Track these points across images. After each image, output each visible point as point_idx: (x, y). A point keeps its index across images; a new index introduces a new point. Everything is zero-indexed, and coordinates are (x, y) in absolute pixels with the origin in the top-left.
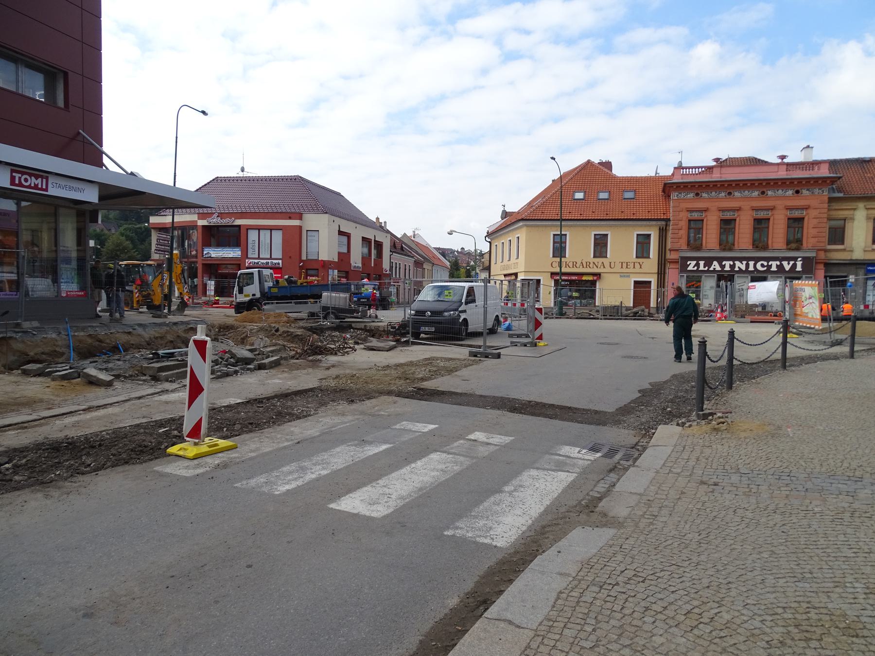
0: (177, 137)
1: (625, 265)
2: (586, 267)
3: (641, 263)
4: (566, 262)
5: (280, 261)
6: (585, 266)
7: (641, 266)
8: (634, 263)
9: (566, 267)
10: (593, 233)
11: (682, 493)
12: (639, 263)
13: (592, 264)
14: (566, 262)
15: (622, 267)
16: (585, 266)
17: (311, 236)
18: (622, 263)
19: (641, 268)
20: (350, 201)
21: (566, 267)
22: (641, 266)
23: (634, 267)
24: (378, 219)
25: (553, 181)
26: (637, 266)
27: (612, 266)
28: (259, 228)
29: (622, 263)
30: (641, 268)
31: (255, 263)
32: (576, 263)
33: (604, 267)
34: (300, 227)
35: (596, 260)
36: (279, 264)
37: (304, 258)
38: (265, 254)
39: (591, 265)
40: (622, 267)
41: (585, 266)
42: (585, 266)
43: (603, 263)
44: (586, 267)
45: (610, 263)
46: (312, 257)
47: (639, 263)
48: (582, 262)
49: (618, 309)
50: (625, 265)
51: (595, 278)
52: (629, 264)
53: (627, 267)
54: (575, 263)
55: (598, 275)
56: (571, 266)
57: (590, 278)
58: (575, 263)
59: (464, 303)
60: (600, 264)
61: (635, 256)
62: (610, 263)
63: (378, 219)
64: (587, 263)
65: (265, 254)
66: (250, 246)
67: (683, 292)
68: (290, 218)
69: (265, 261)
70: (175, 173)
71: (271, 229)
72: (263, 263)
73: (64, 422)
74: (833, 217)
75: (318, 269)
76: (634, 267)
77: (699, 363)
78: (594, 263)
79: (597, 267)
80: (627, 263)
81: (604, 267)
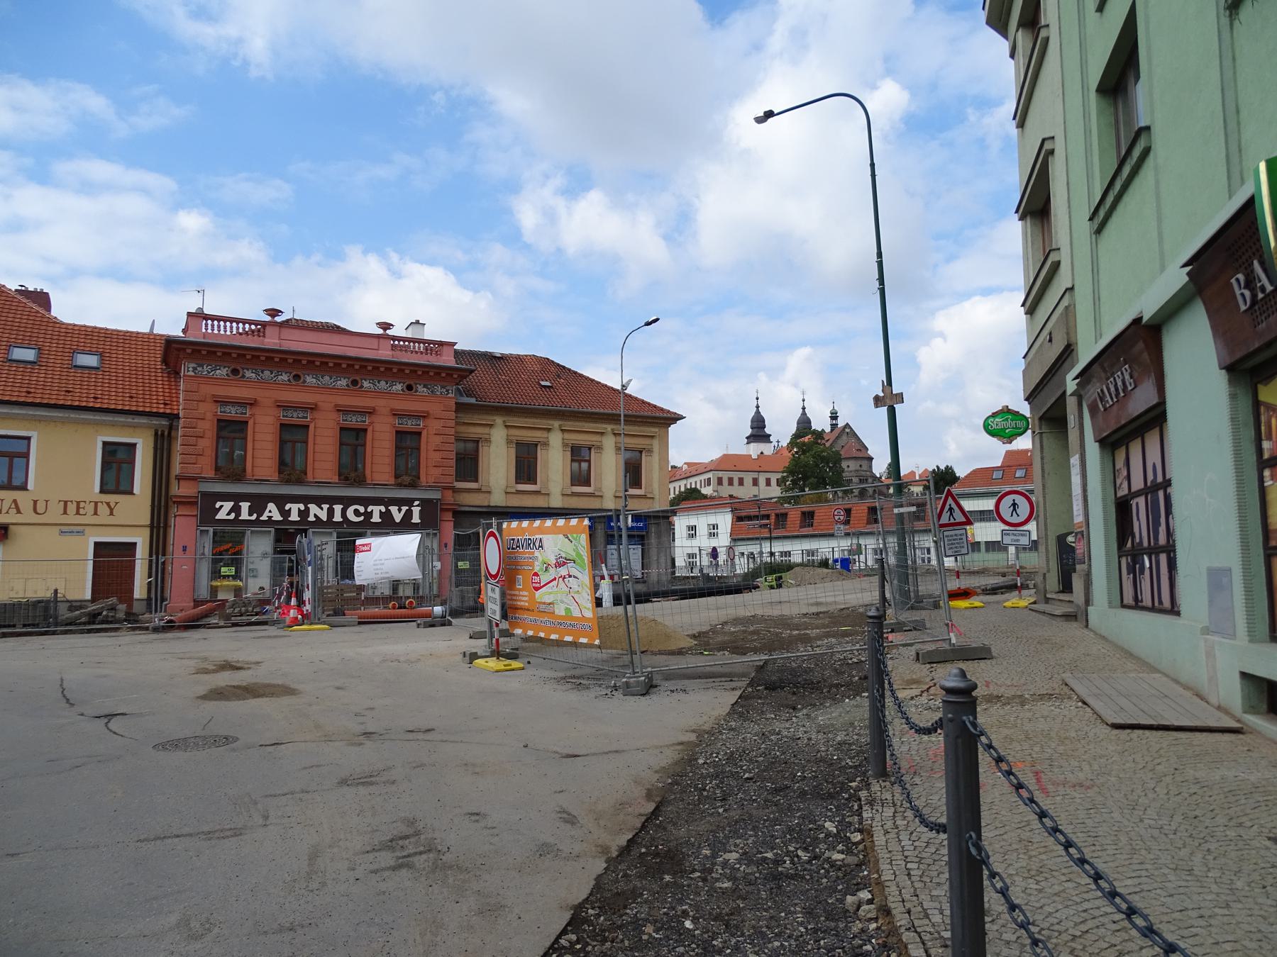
1: (72, 508)
8: (96, 503)
12: (108, 504)
15: (65, 513)
18: (66, 502)
19: (111, 514)
23: (96, 513)
29: (66, 502)
30: (111, 514)
40: (65, 513)
43: (15, 501)
45: (35, 502)
47: (108, 504)
50: (72, 508)
52: (82, 505)
53: (78, 513)
62: (35, 502)
76: (96, 513)
80: (78, 503)
81: (19, 512)
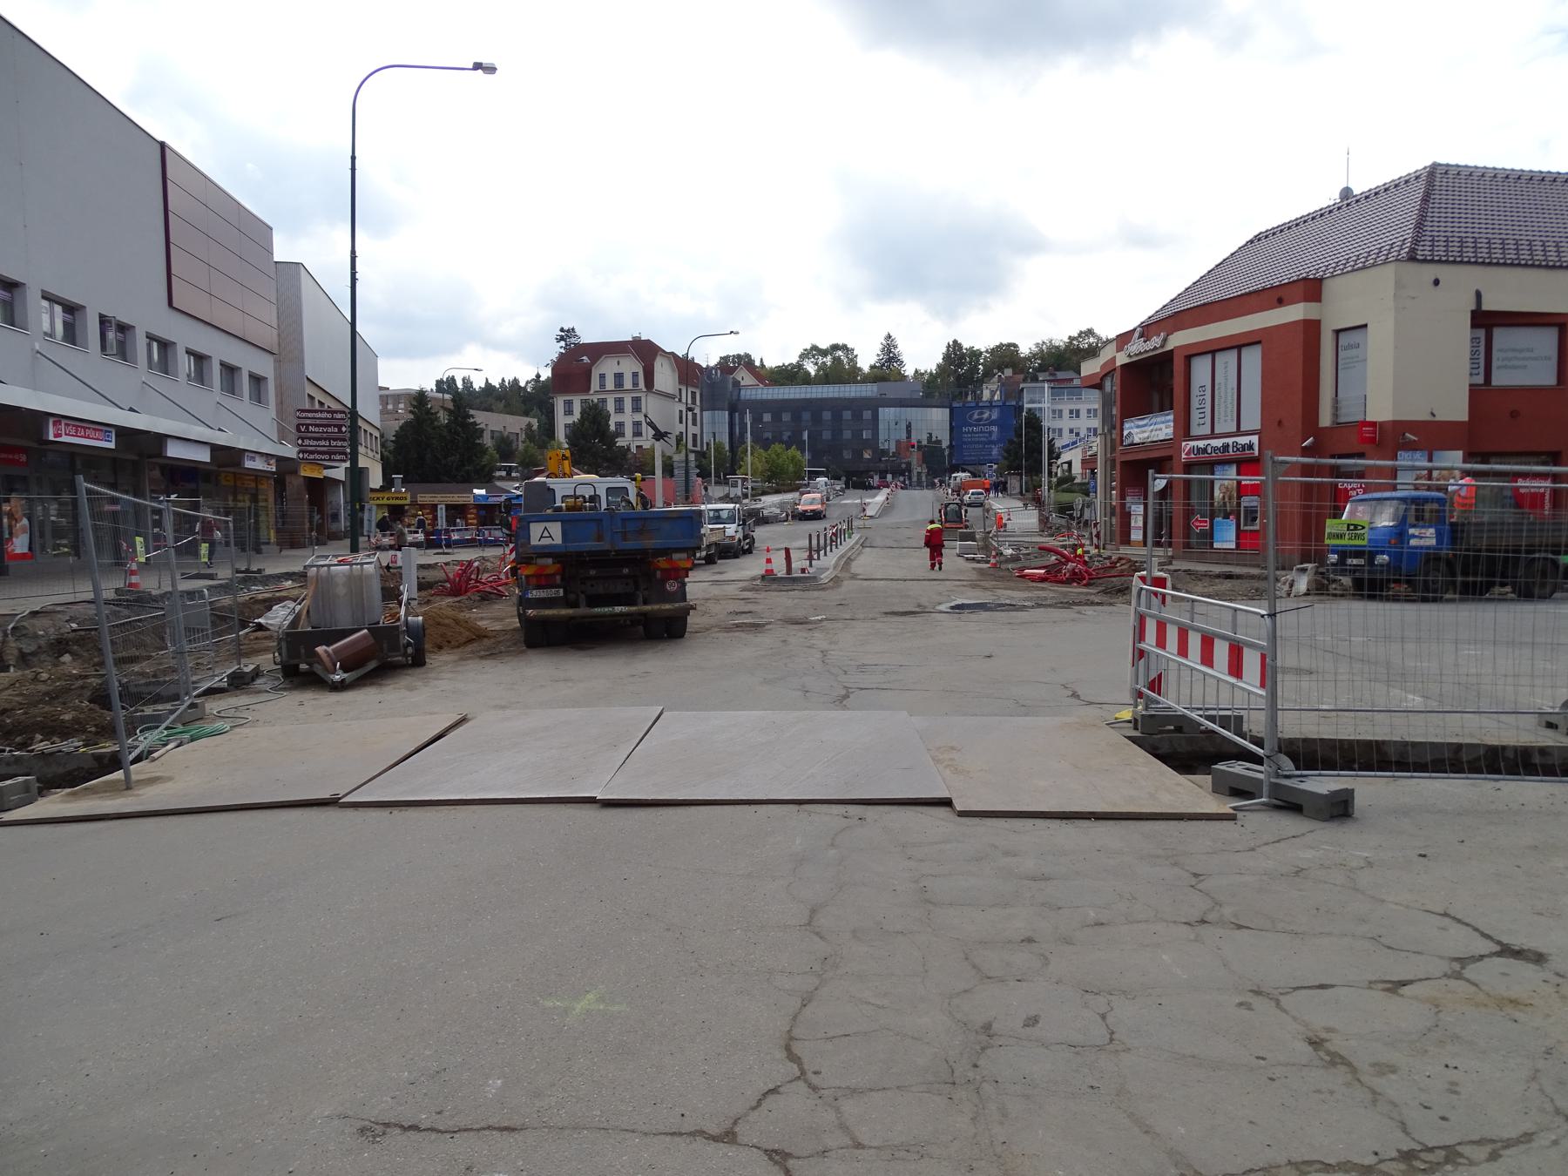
0: (353, 158)
1: (1475, 371)
5: (1255, 439)
11: (1072, 695)
17: (1350, 347)
25: (1346, 193)
28: (1212, 350)
31: (1198, 449)
34: (1311, 329)
36: (1251, 446)
37: (1325, 420)
38: (1226, 424)
46: (1350, 414)
49: (1158, 535)
59: (1482, 758)
65: (1226, 424)
66: (1195, 403)
68: (1281, 302)
69: (1201, 444)
70: (353, 252)
71: (1237, 345)
72: (1215, 449)
73: (37, 687)
74: (1271, 633)
75: (159, 588)
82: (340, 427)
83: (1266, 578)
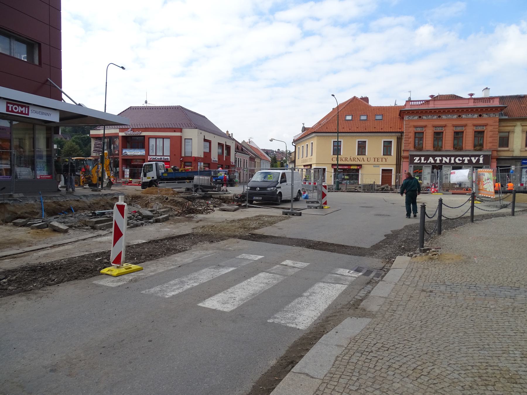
0: (106, 83)
1: (376, 160)
2: (353, 161)
3: (386, 159)
4: (341, 158)
5: (169, 157)
6: (352, 160)
7: (386, 160)
8: (382, 158)
9: (341, 161)
10: (357, 140)
12: (385, 158)
13: (356, 159)
14: (341, 158)
15: (375, 161)
16: (352, 160)
17: (187, 142)
18: (375, 158)
19: (386, 161)
20: (211, 121)
21: (341, 161)
22: (386, 160)
23: (382, 161)
24: (227, 132)
26: (384, 160)
27: (369, 160)
28: (156, 138)
29: (375, 158)
30: (386, 161)
31: (153, 158)
32: (347, 158)
33: (364, 161)
34: (181, 137)
35: (359, 157)
36: (168, 159)
37: (183, 155)
38: (160, 153)
39: (356, 160)
40: (375, 161)
41: (352, 160)
42: (352, 160)
43: (363, 158)
44: (353, 161)
45: (368, 158)
46: (188, 155)
47: (385, 158)
48: (350, 158)
50: (376, 160)
51: (358, 167)
52: (379, 159)
53: (378, 161)
54: (346, 159)
55: (360, 166)
56: (344, 160)
57: (356, 167)
58: (346, 159)
59: (279, 183)
60: (361, 159)
61: (382, 154)
62: (368, 158)
63: (227, 132)
64: (353, 158)
65: (160, 153)
66: (150, 148)
67: (412, 176)
68: (175, 131)
69: (159, 157)
70: (105, 104)
71: (163, 138)
72: (158, 159)
74: (502, 130)
75: (191, 162)
76: (382, 161)
77: (421, 219)
78: (358, 158)
79: (360, 161)
80: (378, 158)
81: (364, 161)
82: (101, 145)
83: (437, 147)
